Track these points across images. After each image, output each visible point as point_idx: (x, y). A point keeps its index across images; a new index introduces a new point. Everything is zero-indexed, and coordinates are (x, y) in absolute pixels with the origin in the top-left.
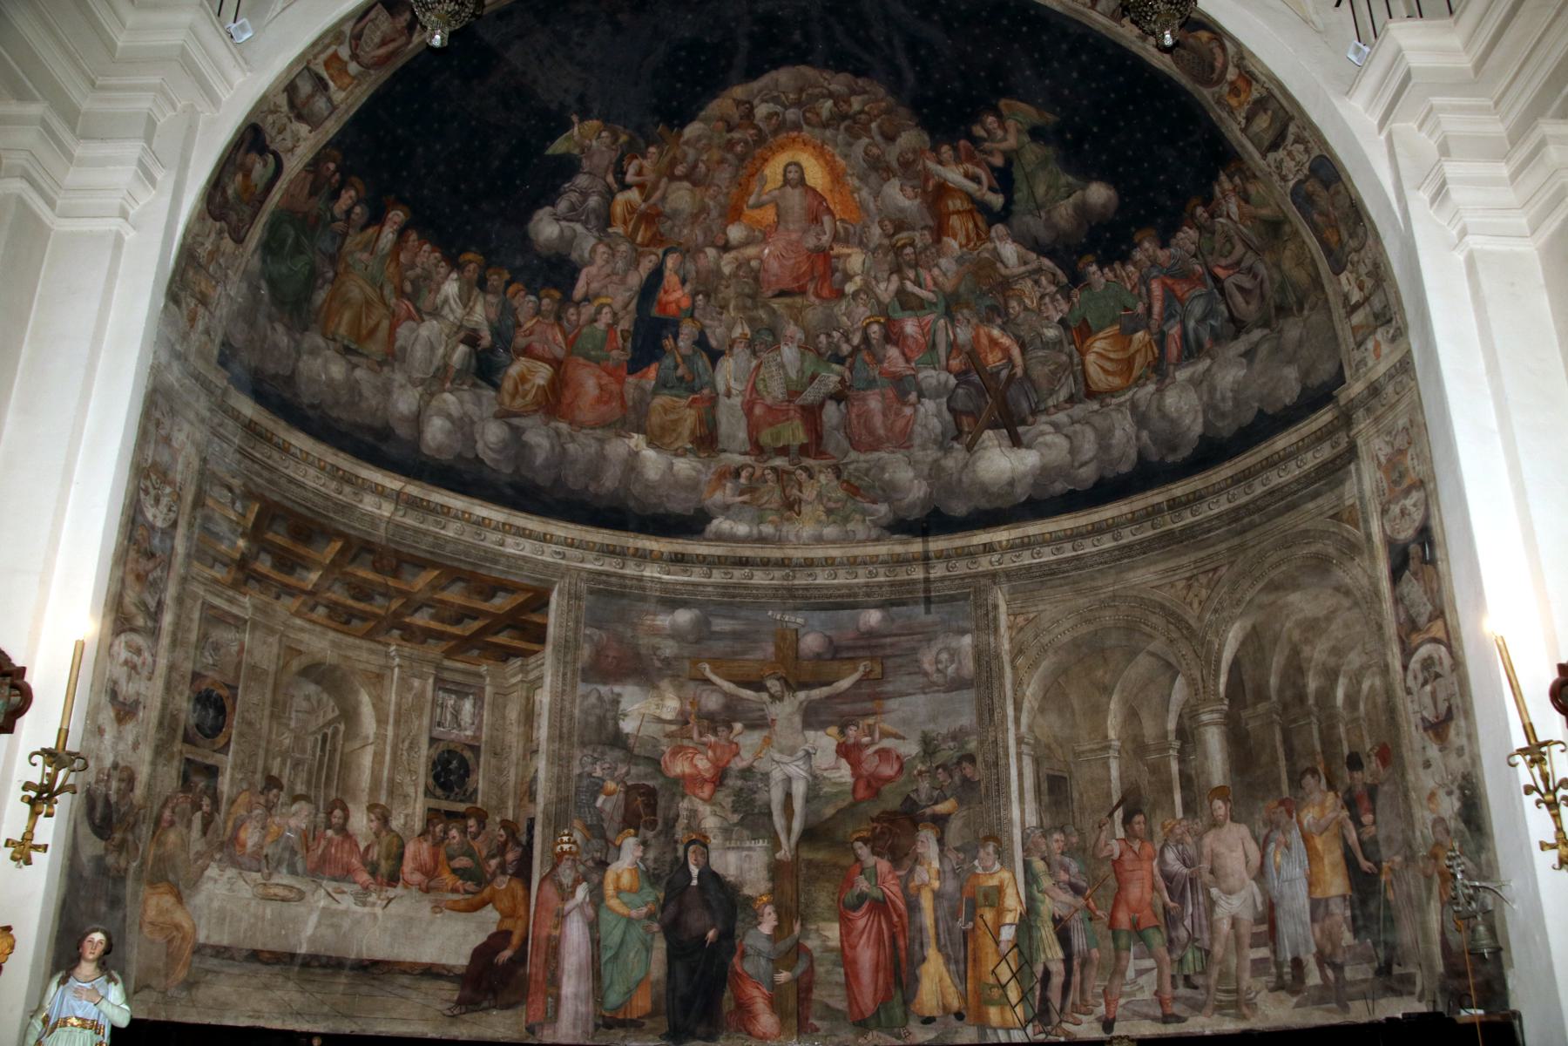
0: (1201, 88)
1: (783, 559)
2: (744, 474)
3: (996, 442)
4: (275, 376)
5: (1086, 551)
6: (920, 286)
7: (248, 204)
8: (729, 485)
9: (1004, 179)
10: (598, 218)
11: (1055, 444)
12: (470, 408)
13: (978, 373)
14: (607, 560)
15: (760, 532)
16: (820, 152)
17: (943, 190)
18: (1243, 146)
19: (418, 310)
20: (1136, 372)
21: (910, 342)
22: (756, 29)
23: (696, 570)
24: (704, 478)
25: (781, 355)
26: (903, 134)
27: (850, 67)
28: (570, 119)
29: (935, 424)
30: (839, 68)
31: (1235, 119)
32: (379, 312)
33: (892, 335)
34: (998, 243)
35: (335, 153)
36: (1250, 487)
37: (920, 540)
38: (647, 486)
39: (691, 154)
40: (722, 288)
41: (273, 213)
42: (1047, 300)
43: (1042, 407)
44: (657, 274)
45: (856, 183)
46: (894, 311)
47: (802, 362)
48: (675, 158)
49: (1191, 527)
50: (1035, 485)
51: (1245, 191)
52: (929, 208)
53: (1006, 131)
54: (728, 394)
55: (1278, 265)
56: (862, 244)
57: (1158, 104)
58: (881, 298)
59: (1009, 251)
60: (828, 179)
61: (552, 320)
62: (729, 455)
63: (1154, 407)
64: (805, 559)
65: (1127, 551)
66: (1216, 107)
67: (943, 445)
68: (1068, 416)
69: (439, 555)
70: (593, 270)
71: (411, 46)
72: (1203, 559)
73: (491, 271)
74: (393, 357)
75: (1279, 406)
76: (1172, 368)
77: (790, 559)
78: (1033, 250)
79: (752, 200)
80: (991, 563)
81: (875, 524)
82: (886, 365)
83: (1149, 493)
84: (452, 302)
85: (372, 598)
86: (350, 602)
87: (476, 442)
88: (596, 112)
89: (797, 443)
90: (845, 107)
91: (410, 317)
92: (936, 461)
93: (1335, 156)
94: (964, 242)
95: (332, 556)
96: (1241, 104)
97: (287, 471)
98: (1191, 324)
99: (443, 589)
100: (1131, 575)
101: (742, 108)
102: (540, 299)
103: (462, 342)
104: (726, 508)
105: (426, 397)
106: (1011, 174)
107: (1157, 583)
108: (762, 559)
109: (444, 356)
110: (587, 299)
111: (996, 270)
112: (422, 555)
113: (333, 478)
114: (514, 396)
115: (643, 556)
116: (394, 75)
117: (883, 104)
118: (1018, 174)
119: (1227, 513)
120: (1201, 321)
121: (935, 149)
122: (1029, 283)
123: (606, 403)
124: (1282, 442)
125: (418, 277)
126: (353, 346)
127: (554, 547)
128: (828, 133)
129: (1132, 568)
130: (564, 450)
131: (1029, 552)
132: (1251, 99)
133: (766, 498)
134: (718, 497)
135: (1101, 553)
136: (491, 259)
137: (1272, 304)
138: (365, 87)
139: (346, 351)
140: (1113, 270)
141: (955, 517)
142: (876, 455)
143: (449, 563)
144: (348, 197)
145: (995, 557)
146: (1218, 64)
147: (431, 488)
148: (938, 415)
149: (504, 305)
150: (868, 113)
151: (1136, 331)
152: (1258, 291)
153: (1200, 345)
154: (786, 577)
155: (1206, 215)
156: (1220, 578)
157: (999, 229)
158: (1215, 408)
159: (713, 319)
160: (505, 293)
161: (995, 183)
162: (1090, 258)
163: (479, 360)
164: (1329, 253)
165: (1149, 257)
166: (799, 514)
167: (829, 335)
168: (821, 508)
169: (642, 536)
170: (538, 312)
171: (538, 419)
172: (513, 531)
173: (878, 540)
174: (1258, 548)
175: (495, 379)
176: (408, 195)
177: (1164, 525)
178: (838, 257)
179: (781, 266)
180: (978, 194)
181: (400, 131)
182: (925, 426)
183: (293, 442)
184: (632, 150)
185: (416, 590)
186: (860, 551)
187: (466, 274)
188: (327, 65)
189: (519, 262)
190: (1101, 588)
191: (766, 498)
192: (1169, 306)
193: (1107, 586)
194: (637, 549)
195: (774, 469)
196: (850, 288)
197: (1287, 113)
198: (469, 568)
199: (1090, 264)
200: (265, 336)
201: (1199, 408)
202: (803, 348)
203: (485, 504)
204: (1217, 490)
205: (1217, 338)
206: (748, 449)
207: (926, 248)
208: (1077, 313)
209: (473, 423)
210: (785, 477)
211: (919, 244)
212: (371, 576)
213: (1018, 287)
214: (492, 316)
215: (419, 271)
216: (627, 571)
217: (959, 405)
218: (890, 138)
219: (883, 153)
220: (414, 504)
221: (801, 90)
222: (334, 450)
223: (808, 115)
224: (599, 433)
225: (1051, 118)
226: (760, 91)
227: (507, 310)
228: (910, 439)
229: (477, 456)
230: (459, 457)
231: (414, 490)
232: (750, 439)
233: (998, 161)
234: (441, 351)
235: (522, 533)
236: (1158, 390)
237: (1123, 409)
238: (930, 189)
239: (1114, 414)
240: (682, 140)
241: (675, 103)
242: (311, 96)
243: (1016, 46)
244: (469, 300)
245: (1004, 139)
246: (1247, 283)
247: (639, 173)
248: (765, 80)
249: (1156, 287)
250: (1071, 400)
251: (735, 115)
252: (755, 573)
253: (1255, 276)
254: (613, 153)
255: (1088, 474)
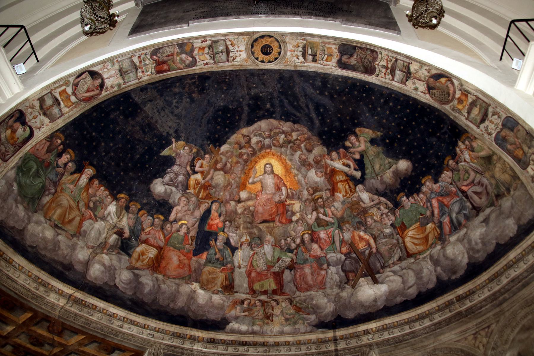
0: (445, 106)
1: (264, 343)
2: (246, 303)
3: (366, 283)
4: (13, 228)
5: (417, 328)
6: (326, 216)
7: (12, 145)
8: (238, 308)
9: (360, 164)
10: (182, 185)
11: (395, 280)
12: (115, 263)
13: (355, 253)
14: (175, 340)
15: (253, 329)
16: (280, 158)
17: (334, 172)
18: (468, 126)
19: (95, 216)
20: (430, 242)
21: (323, 241)
22: (251, 102)
23: (220, 347)
24: (226, 304)
25: (263, 249)
26: (315, 148)
27: (291, 119)
28: (171, 140)
29: (336, 278)
30: (286, 120)
31: (462, 115)
32: (75, 213)
33: (314, 239)
34: (360, 193)
35: (61, 135)
36: (499, 281)
37: (332, 331)
38: (198, 306)
39: (224, 159)
40: (237, 219)
41: (26, 154)
42: (384, 216)
43: (387, 264)
44: (208, 212)
45: (296, 172)
46: (315, 227)
47: (274, 253)
48: (217, 160)
49: (471, 308)
50: (387, 300)
51: (471, 146)
52: (328, 180)
53: (359, 142)
54: (240, 267)
55: (493, 177)
56: (299, 199)
57: (426, 119)
58: (309, 223)
59: (365, 196)
60: (284, 170)
61: (159, 229)
62: (238, 294)
63: (441, 254)
64: (275, 342)
65: (439, 325)
66: (453, 112)
67: (341, 286)
68: (399, 267)
69: (86, 328)
70: (179, 208)
71: (101, 96)
72: (480, 323)
73: (132, 203)
74: (79, 233)
75: (507, 239)
76: (447, 236)
77: (267, 342)
78: (376, 194)
79: (251, 181)
80: (368, 339)
81: (309, 324)
82: (312, 252)
83: (445, 295)
84: (112, 215)
85: (43, 345)
86: (29, 346)
87: (116, 278)
88: (183, 138)
89: (271, 289)
90: (290, 138)
91: (91, 218)
92: (338, 294)
93: (514, 114)
94: (345, 194)
95: (24, 320)
96: (464, 107)
97: (8, 273)
98: (454, 215)
99: (86, 345)
100: (442, 337)
101: (246, 138)
102: (154, 219)
103: (115, 233)
104: (237, 318)
105: (93, 255)
106: (364, 161)
107: (456, 339)
108: (253, 342)
109: (105, 238)
110: (176, 221)
111: (360, 205)
112: (77, 327)
113: (35, 282)
114: (137, 261)
115: (194, 339)
116: (93, 107)
117: (306, 136)
118: (366, 162)
119: (489, 297)
120: (459, 212)
121: (329, 154)
122: (376, 209)
123: (182, 268)
124: (512, 255)
125: (97, 201)
126: (60, 225)
127: (149, 332)
128: (283, 150)
129: (442, 334)
130: (159, 287)
131: (387, 332)
132: (468, 103)
133: (256, 314)
134: (233, 313)
135: (425, 328)
136: (132, 197)
137: (493, 195)
138: (78, 109)
139: (56, 226)
140: (413, 198)
141: (348, 319)
142: (309, 293)
143: (91, 333)
144: (65, 158)
145: (370, 336)
146: (451, 92)
147: (88, 295)
148: (338, 273)
149: (137, 219)
150: (300, 140)
151: (428, 224)
152: (485, 191)
153: (460, 224)
154: (265, 351)
155: (454, 163)
156: (492, 331)
157: (360, 187)
158: (472, 249)
159: (233, 232)
160: (138, 214)
161: (357, 167)
162: (402, 194)
163: (122, 242)
164: (518, 160)
165: (429, 189)
166: (272, 321)
167: (286, 240)
168: (283, 318)
169: (194, 329)
170: (153, 224)
171: (148, 272)
172: (128, 321)
173: (311, 332)
174: (511, 310)
175: (129, 252)
176: (95, 163)
177: (456, 309)
178: (289, 205)
179: (264, 209)
180: (349, 172)
181: (94, 134)
182: (332, 279)
183: (16, 260)
184: (198, 156)
185: (70, 344)
186: (301, 338)
187: (120, 203)
188: (60, 93)
189: (145, 201)
190: (427, 346)
191: (256, 314)
192: (442, 210)
193: (430, 344)
194: (191, 336)
195: (260, 301)
196: (294, 218)
197: (487, 103)
198: (102, 337)
199: (402, 197)
200: (11, 209)
201: (465, 251)
202: (274, 246)
203: (116, 307)
204: (482, 287)
205: (468, 218)
206: (248, 291)
207: (328, 198)
208: (399, 220)
209: (115, 269)
210: (266, 304)
211: (325, 197)
212: (45, 333)
213: (370, 212)
214: (131, 224)
215: (97, 198)
216: (185, 346)
217: (347, 268)
218: (310, 151)
219: (307, 158)
220: (78, 302)
221: (271, 130)
222: (39, 269)
223: (274, 142)
224: (177, 281)
225: (379, 134)
226: (253, 131)
227: (138, 222)
228: (325, 285)
229: (115, 284)
230: (106, 283)
231: (79, 295)
232: (249, 287)
233: (357, 156)
234: (104, 236)
235: (133, 323)
236: (442, 248)
237: (426, 259)
238: (328, 172)
239: (422, 262)
240: (220, 152)
241: (217, 136)
242: (52, 106)
243: (361, 103)
244: (120, 215)
245: (359, 146)
246: (478, 189)
247: (201, 167)
248: (256, 126)
249: (435, 202)
250: (400, 259)
251: (243, 141)
252: (250, 349)
253: (482, 185)
254: (190, 157)
255: (413, 292)
